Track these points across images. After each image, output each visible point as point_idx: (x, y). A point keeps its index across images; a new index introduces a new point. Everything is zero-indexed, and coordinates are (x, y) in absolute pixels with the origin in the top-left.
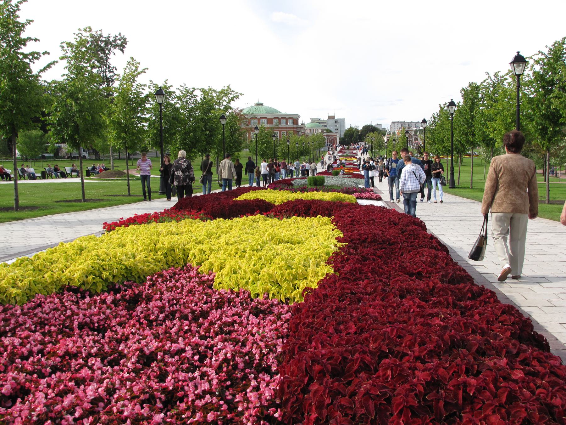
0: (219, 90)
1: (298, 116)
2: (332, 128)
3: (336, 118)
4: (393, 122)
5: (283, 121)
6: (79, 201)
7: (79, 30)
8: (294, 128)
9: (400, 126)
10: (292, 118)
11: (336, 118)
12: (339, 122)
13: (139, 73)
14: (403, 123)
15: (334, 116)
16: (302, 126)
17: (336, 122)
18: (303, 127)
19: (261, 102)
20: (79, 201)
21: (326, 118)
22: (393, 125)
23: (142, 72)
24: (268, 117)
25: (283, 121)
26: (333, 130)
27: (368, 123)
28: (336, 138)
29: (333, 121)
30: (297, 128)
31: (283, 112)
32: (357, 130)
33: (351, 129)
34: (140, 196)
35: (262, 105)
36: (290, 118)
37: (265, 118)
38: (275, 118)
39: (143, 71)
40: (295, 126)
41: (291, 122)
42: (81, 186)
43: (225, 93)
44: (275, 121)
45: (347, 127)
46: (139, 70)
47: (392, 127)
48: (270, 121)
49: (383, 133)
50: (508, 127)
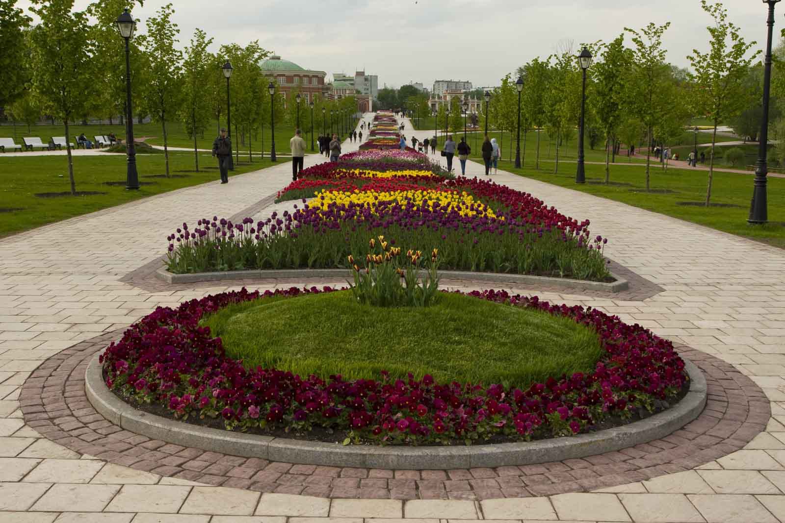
0: (244, 47)
1: (324, 74)
2: (360, 88)
3: (366, 74)
4: (437, 82)
5: (306, 80)
6: (163, 176)
7: (163, 8)
8: (319, 89)
9: (445, 85)
10: (317, 76)
11: (366, 74)
12: (370, 80)
13: (207, 45)
14: (449, 83)
15: (363, 73)
16: (329, 86)
17: (366, 79)
18: (328, 88)
19: (277, 55)
20: (163, 176)
21: (352, 74)
22: (437, 84)
23: (209, 43)
24: (287, 74)
25: (306, 80)
26: (363, 92)
27: (407, 83)
28: (368, 101)
29: (361, 79)
30: (323, 89)
31: (305, 68)
32: (393, 91)
33: (386, 90)
34: (572, 158)
35: (278, 58)
36: (314, 76)
37: (284, 75)
38: (295, 76)
39: (210, 42)
40: (320, 86)
41: (315, 81)
42: (68, 157)
43: (251, 50)
44: (296, 79)
45: (381, 86)
46: (206, 40)
47: (436, 86)
48: (290, 79)
49: (425, 95)
50: (573, 110)
